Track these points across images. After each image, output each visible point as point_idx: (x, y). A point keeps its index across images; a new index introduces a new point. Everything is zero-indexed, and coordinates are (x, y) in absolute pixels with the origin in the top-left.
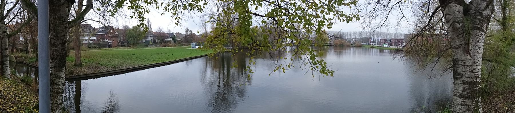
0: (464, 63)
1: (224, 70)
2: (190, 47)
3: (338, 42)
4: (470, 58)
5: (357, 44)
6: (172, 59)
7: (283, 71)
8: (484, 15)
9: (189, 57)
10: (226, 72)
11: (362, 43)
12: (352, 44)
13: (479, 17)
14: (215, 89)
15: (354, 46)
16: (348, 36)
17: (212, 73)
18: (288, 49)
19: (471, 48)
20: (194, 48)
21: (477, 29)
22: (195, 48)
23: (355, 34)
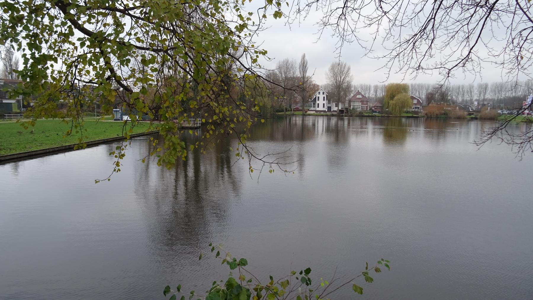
1: (186, 171)
2: (94, 119)
3: (434, 108)
5: (335, 123)
6: (52, 144)
7: (189, 298)
9: (97, 139)
10: (191, 173)
11: (500, 111)
12: (473, 114)
14: (166, 208)
15: (476, 119)
16: (463, 94)
17: (162, 177)
18: (321, 123)
20: (119, 120)
22: (122, 120)
23: (484, 88)
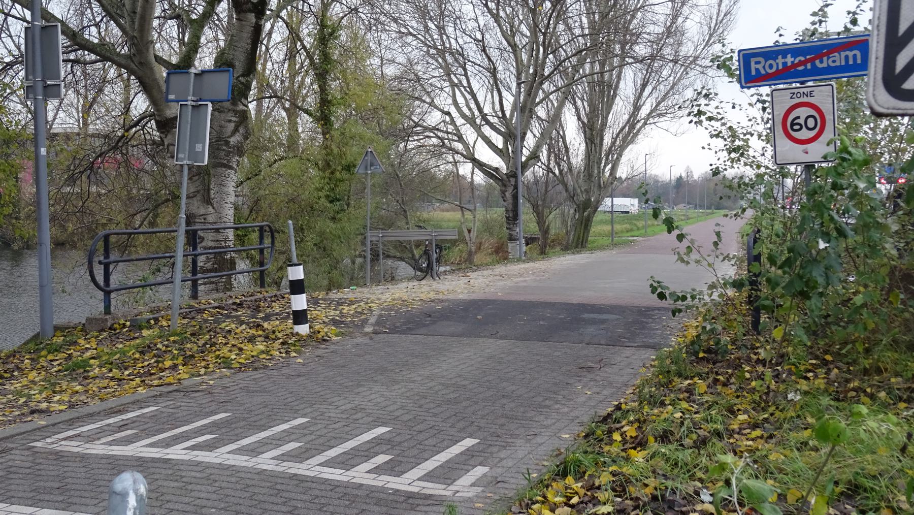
0: (205, 219)
4: (213, 211)
8: (232, 143)
13: (225, 148)
19: (213, 196)
21: (221, 166)
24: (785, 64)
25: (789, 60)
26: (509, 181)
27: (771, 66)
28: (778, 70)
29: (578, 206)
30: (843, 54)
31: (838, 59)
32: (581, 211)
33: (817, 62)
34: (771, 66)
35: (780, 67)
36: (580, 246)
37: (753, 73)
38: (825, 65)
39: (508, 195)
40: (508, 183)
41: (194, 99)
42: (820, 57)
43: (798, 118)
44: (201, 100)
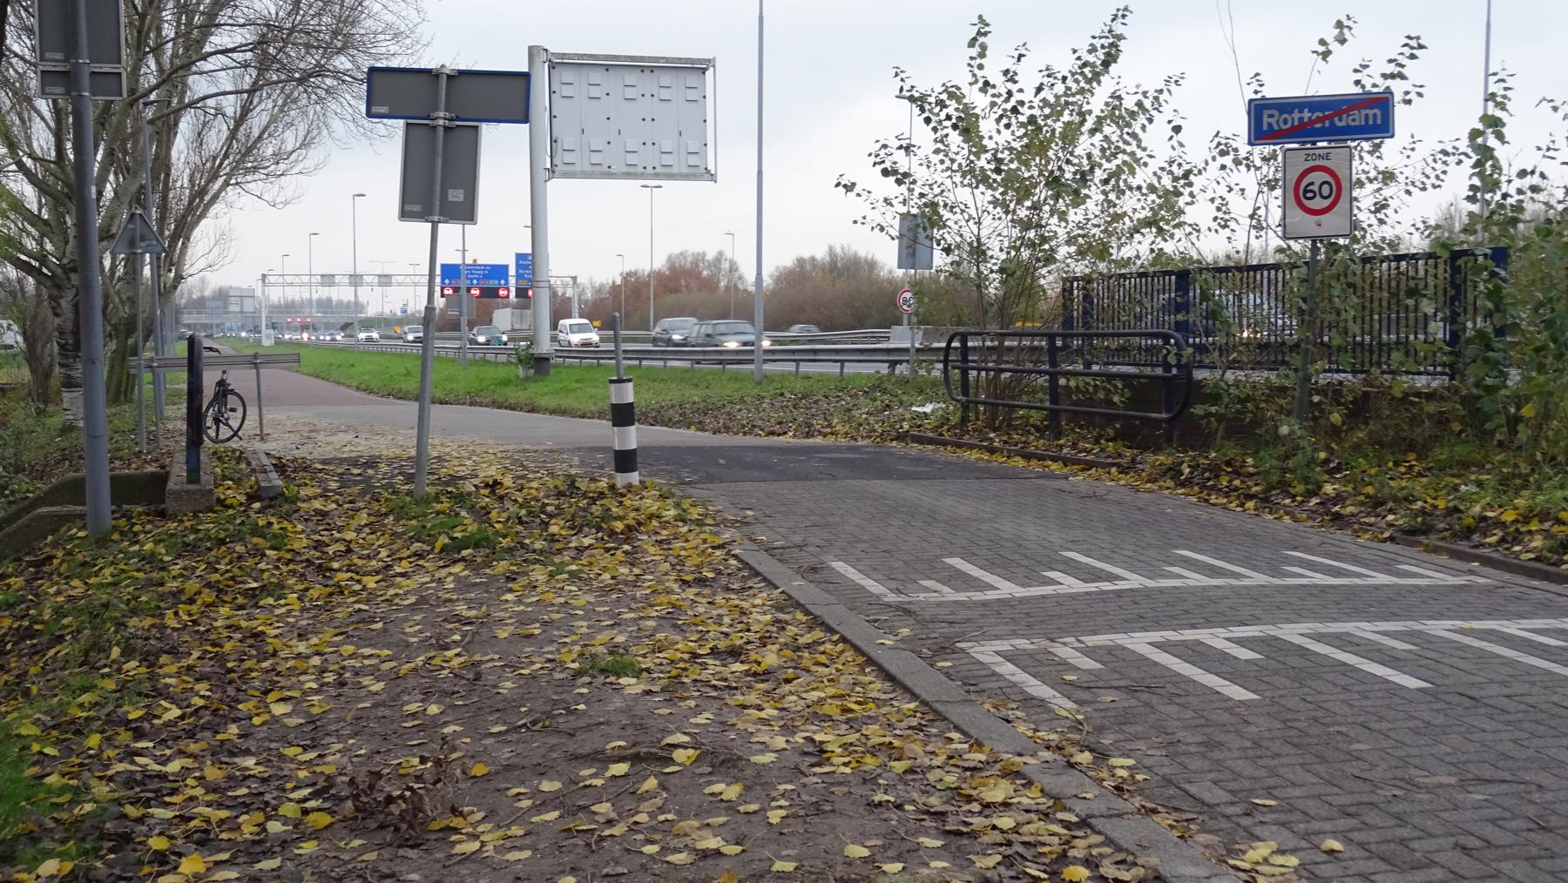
24: (1301, 119)
25: (1306, 115)
26: (69, 278)
27: (1285, 121)
28: (1293, 127)
29: (115, 327)
30: (1364, 112)
31: (1357, 118)
32: (122, 336)
33: (1336, 119)
34: (1285, 121)
35: (1296, 123)
36: (122, 398)
37: (1265, 128)
38: (1343, 124)
39: (65, 304)
40: (65, 282)
41: (448, 115)
42: (1339, 113)
43: (1312, 184)
44: (458, 119)
